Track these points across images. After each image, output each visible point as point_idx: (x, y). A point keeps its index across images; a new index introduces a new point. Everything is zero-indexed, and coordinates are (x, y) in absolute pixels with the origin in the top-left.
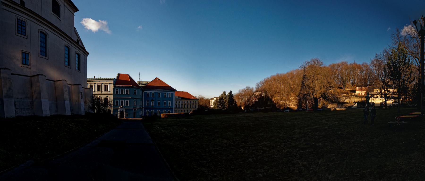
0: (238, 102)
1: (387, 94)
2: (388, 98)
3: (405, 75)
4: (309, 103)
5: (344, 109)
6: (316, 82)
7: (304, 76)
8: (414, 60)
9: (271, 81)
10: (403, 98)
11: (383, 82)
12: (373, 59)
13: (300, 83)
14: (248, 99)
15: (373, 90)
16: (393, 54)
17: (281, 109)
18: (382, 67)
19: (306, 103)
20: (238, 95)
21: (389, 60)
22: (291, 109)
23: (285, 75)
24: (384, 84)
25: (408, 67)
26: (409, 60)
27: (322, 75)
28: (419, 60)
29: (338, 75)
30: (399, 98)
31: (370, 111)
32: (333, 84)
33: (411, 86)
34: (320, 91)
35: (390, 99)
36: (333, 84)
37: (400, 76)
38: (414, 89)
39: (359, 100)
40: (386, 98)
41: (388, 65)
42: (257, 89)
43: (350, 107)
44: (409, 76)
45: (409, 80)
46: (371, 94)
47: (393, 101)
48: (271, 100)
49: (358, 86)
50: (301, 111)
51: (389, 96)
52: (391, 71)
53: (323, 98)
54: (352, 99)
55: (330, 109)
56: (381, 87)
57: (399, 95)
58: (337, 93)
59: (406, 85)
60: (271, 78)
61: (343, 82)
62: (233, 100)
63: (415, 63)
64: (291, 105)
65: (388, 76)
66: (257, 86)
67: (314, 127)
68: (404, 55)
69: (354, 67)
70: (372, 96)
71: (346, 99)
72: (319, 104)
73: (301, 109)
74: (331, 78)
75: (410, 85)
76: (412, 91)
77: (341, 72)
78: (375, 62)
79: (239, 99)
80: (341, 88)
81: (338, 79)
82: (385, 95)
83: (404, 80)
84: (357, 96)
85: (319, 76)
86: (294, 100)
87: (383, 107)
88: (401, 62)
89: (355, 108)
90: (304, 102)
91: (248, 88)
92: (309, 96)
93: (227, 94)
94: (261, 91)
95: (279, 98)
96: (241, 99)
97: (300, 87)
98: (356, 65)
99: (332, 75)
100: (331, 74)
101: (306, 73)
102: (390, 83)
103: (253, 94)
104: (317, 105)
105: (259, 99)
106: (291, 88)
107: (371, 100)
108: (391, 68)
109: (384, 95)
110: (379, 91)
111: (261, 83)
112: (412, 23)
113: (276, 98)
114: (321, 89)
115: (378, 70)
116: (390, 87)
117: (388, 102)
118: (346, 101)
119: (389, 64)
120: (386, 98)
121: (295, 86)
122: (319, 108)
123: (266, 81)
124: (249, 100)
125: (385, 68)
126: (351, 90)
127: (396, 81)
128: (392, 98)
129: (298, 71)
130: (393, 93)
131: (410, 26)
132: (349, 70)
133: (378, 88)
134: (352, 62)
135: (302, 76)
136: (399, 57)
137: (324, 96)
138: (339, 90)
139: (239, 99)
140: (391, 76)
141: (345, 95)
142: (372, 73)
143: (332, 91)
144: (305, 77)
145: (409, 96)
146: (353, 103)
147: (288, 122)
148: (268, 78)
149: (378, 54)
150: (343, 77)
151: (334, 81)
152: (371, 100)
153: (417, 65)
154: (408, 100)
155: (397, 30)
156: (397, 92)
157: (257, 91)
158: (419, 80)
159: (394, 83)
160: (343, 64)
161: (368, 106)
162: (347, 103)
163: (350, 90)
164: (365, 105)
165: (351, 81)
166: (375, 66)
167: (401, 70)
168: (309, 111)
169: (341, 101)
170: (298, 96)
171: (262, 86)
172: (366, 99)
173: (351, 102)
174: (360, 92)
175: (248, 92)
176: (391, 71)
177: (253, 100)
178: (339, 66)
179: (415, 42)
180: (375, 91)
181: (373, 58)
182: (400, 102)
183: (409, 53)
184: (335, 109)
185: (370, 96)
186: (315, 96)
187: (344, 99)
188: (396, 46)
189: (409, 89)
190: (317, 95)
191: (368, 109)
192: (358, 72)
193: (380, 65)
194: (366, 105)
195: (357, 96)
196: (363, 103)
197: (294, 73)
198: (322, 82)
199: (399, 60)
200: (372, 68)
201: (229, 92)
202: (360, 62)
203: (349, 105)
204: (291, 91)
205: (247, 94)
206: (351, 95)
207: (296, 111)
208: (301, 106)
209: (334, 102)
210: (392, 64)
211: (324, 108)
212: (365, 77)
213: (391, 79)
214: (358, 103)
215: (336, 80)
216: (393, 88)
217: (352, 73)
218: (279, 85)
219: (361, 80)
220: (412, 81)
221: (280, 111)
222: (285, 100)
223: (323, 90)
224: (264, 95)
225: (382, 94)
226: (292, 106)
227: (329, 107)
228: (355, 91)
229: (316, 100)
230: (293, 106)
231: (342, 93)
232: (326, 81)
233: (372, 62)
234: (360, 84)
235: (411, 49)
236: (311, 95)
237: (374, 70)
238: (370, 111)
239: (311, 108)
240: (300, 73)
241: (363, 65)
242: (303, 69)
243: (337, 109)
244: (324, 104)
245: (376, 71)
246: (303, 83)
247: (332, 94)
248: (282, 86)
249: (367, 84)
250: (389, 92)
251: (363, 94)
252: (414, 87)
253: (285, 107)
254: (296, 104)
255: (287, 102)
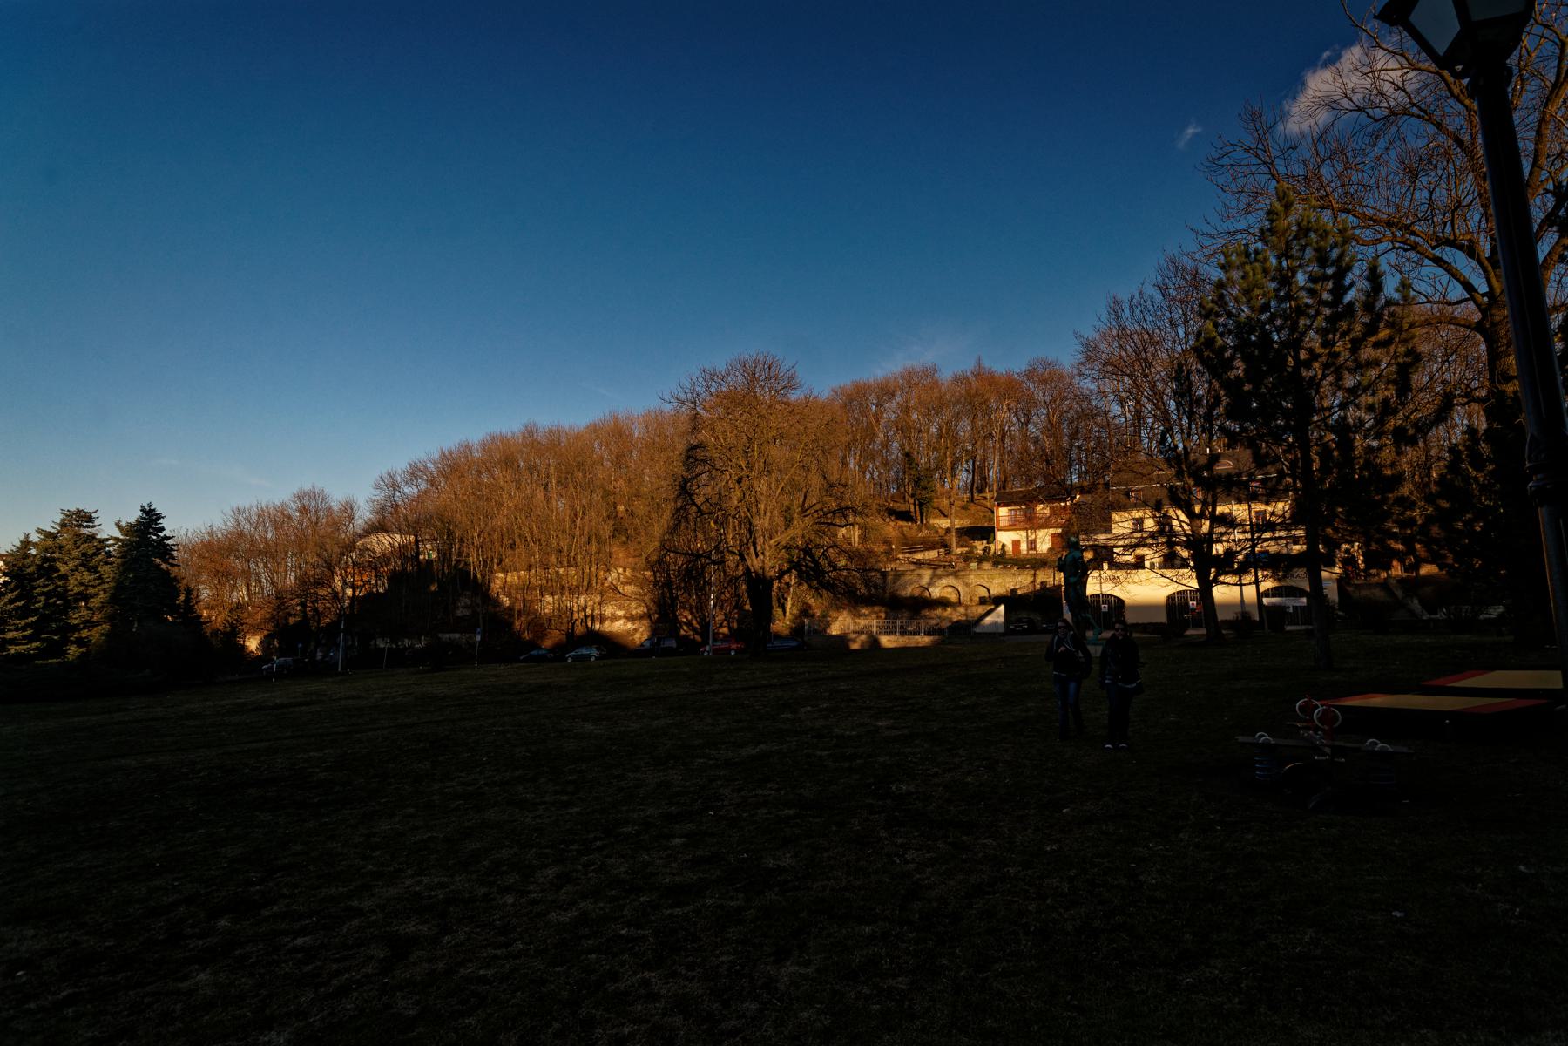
0: (211, 601)
1: (1210, 539)
2: (1225, 564)
3: (1353, 392)
4: (720, 603)
5: (924, 640)
6: (761, 486)
7: (692, 448)
8: (1430, 269)
9: (485, 466)
10: (1350, 561)
11: (1178, 461)
12: (1090, 334)
13: (667, 490)
14: (302, 581)
15: (1109, 520)
16: (1236, 275)
17: (548, 643)
18: (1159, 370)
19: (701, 606)
20: (222, 553)
21: (1206, 314)
22: (611, 646)
23: (578, 437)
24: (1179, 475)
25: (1371, 329)
26: (1374, 277)
27: (794, 448)
28: (1471, 251)
29: (886, 445)
30: (1312, 562)
31: (1096, 651)
32: (861, 491)
33: (1415, 466)
34: (783, 538)
35: (1242, 570)
36: (855, 498)
37: (1306, 408)
38: (1452, 487)
39: (1021, 582)
40: (1208, 567)
41: (1206, 351)
42: (381, 510)
43: (964, 629)
44: (1390, 393)
45: (1391, 423)
46: (1094, 548)
47: (1267, 585)
48: (480, 590)
49: (1003, 500)
50: (670, 652)
51: (1230, 554)
52: (1232, 387)
53: (803, 577)
54: (973, 579)
55: (843, 640)
56: (1163, 495)
57: (1311, 540)
58: (879, 548)
59: (1368, 464)
60: (487, 447)
61: (917, 482)
62: (169, 584)
63: (1439, 286)
64: (614, 618)
65: (1209, 417)
66: (380, 495)
67: (751, 751)
68: (1322, 260)
69: (978, 394)
70: (1104, 556)
71: (935, 577)
72: (778, 611)
73: (673, 644)
74: (845, 464)
75: (1411, 454)
76: (1430, 499)
77: (903, 428)
78: (1109, 349)
79: (224, 577)
80: (905, 516)
81: (886, 464)
82: (1199, 545)
83: (1344, 430)
84: (1002, 561)
85: (778, 453)
86: (629, 589)
87: (1186, 625)
88: (1301, 311)
89: (992, 636)
90: (693, 601)
91: (308, 504)
92: (722, 562)
93: (107, 529)
94: (414, 527)
95: (536, 577)
96: (246, 575)
97: (667, 514)
98: (990, 380)
99: (848, 447)
100: (845, 439)
101: (704, 435)
102: (1225, 466)
103: (350, 547)
104: (769, 618)
105: (395, 578)
106: (612, 514)
107: (1095, 585)
108: (1228, 365)
109: (1186, 545)
110: (1149, 524)
111: (413, 474)
112: (1372, 25)
113: (512, 578)
114: (788, 522)
115: (1135, 392)
116: (1236, 487)
117: (1220, 593)
118: (936, 592)
119: (1210, 342)
120: (1208, 567)
121: (640, 507)
122: (777, 636)
123: (454, 467)
124: (307, 586)
125: (1180, 375)
126: (967, 523)
127: (1278, 440)
128: (1255, 562)
129: (656, 422)
130: (1263, 525)
131: (1354, 54)
132: (947, 414)
133: (1144, 504)
134: (966, 366)
135: (681, 447)
136: (1285, 279)
137: (809, 566)
138: (891, 528)
139: (224, 577)
140: (1229, 415)
141: (932, 554)
142: (1091, 414)
143: (850, 534)
144: (700, 454)
145: (1408, 541)
146: (983, 601)
147: (589, 726)
148: (467, 448)
149: (1124, 297)
150: (915, 458)
151: (862, 480)
152: (1095, 585)
153: (1457, 292)
154: (1397, 570)
155: (1254, 118)
156: (1295, 519)
157: (379, 527)
158: (1498, 407)
159: (1261, 461)
160: (911, 380)
161: (1081, 624)
162: (943, 603)
163: (958, 524)
164: (1056, 615)
165: (963, 477)
166: (1113, 368)
167: (1307, 364)
168: (715, 651)
169: (908, 591)
170: (658, 565)
171: (422, 496)
172: (1060, 577)
173: (965, 598)
174: (1021, 536)
175: (312, 534)
176: (1227, 385)
177: (345, 587)
178: (886, 391)
179: (1417, 136)
180: (1122, 523)
181: (1093, 324)
182: (1331, 591)
183: (1368, 234)
184: (874, 642)
185: (1088, 555)
186: (755, 563)
187: (925, 580)
188: (1256, 220)
189: (1405, 490)
190: (765, 560)
191: (1080, 642)
192: (1005, 416)
193: (1142, 359)
194: (1068, 616)
195: (1002, 561)
196: (1043, 600)
197: (637, 431)
198: (794, 486)
199: (1289, 297)
200: (1089, 385)
201: (133, 516)
202: (1009, 362)
203: (956, 615)
204: (617, 531)
205: (301, 544)
206: (967, 558)
207: (640, 652)
208: (674, 624)
209: (868, 601)
210: (1230, 341)
211: (808, 637)
212: (1048, 444)
213: (1233, 440)
214: (1011, 601)
215: (874, 471)
216: (1252, 498)
217: (964, 429)
218: (540, 494)
219: (1024, 466)
220: (1423, 428)
221: (540, 660)
222: (575, 590)
223: (800, 529)
224: (430, 552)
225: (1170, 544)
226: (619, 626)
227: (835, 630)
228: (987, 533)
229: (760, 587)
230: (623, 621)
231: (914, 545)
232: (815, 480)
233: (1090, 352)
234: (1017, 487)
235: (1377, 203)
236: (731, 561)
237: (1103, 395)
238: (1096, 651)
239: (734, 635)
240: (670, 431)
241: (1030, 374)
242: (685, 411)
243: (887, 641)
244: (805, 611)
245: (1122, 402)
246: (684, 489)
247: (852, 555)
248: (561, 505)
249: (1062, 483)
250: (1229, 521)
251: (1044, 542)
252: (1453, 466)
253: (570, 634)
254: (642, 610)
255: (589, 601)
